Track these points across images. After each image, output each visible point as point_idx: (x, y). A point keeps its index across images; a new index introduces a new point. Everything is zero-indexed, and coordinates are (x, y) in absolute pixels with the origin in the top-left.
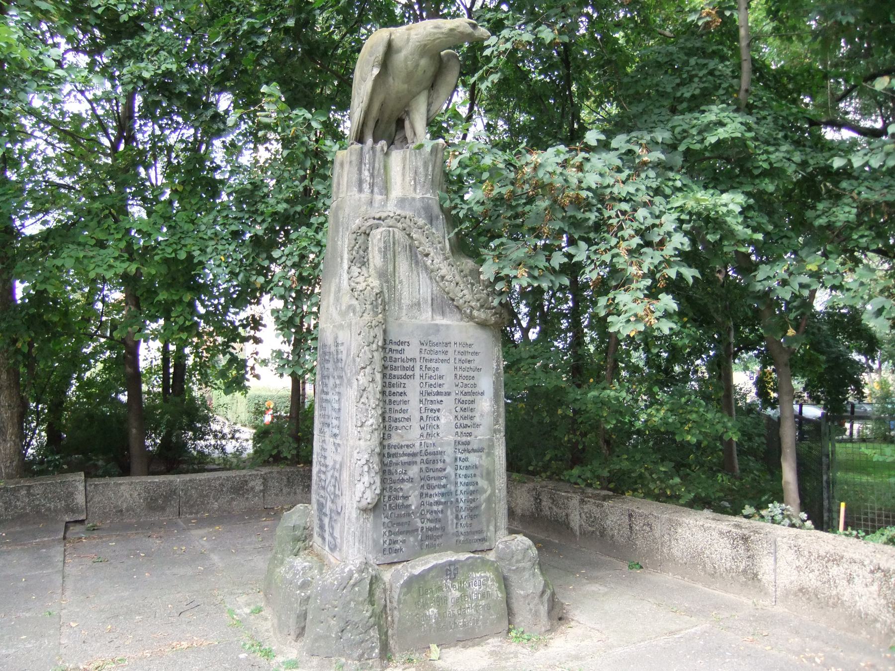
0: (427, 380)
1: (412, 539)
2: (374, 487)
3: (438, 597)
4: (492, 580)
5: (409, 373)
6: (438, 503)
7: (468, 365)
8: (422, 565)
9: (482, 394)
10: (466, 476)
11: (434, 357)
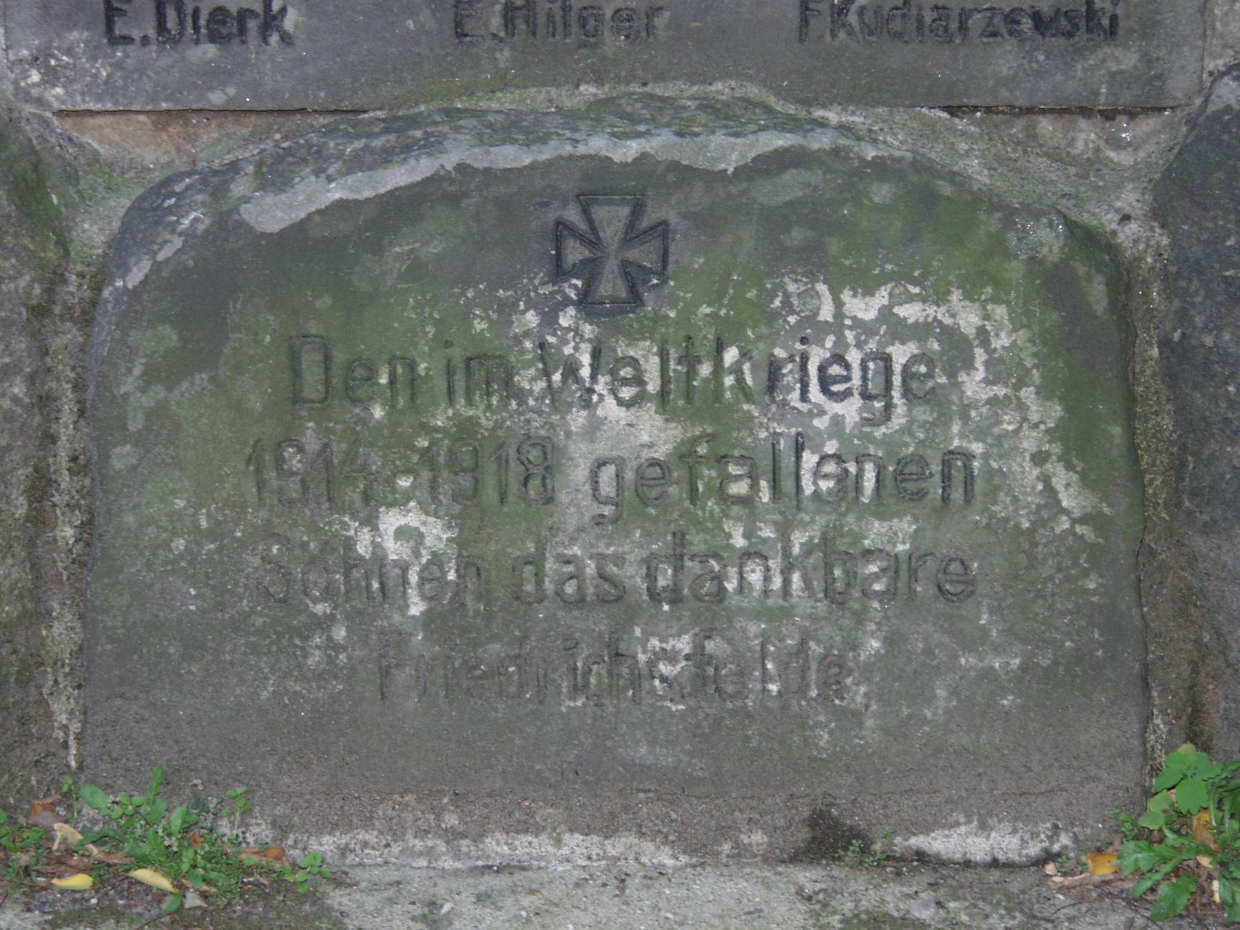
3: (466, 428)
4: (998, 370)
8: (356, 163)
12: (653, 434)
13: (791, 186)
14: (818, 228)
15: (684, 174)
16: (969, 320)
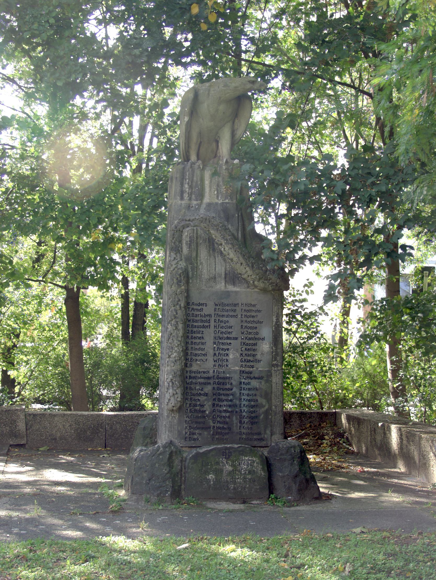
3: (216, 468)
12: (230, 468)
13: (241, 449)
14: (243, 452)
15: (233, 448)
16: (255, 459)
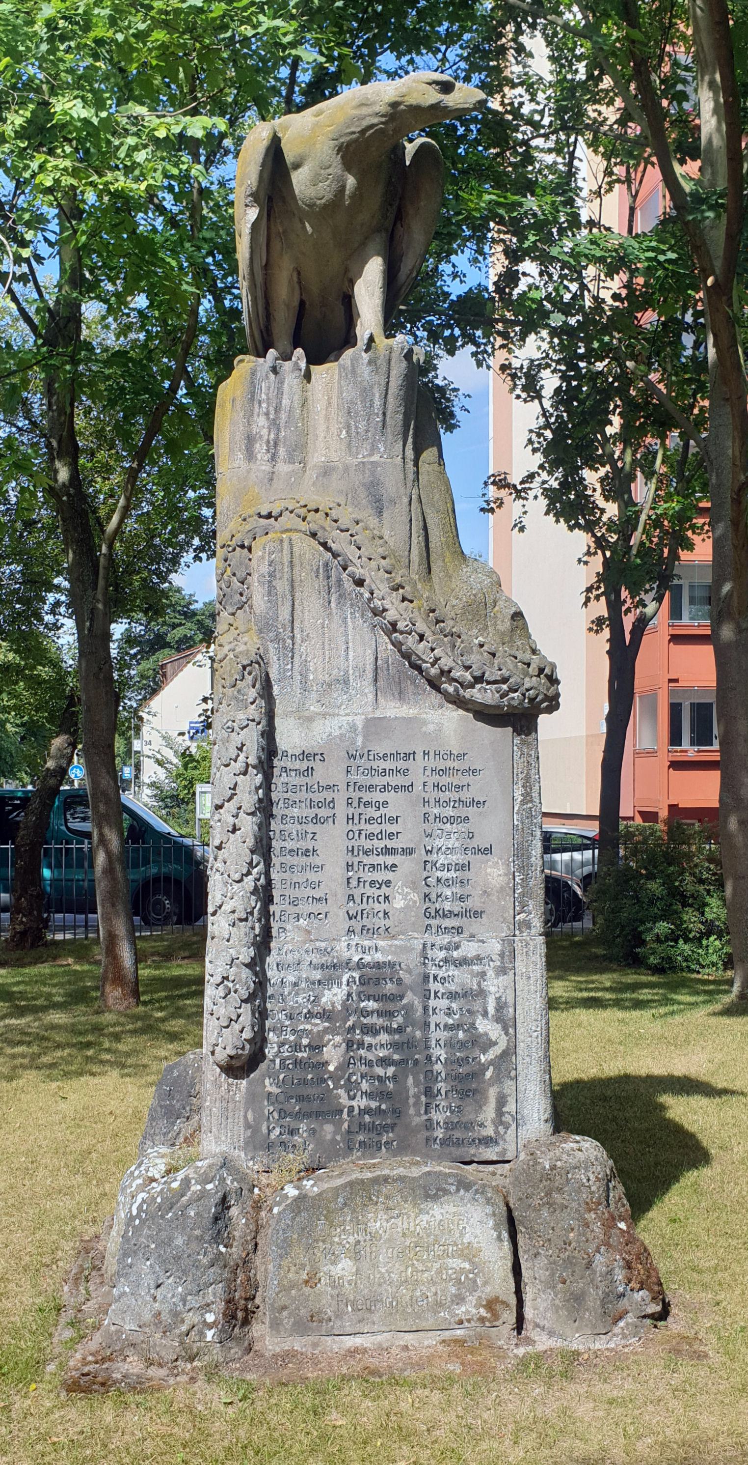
0: (363, 826)
1: (329, 1128)
2: (237, 1027)
5: (323, 813)
6: (384, 1062)
7: (454, 796)
9: (488, 851)
10: (449, 1012)
11: (379, 781)
